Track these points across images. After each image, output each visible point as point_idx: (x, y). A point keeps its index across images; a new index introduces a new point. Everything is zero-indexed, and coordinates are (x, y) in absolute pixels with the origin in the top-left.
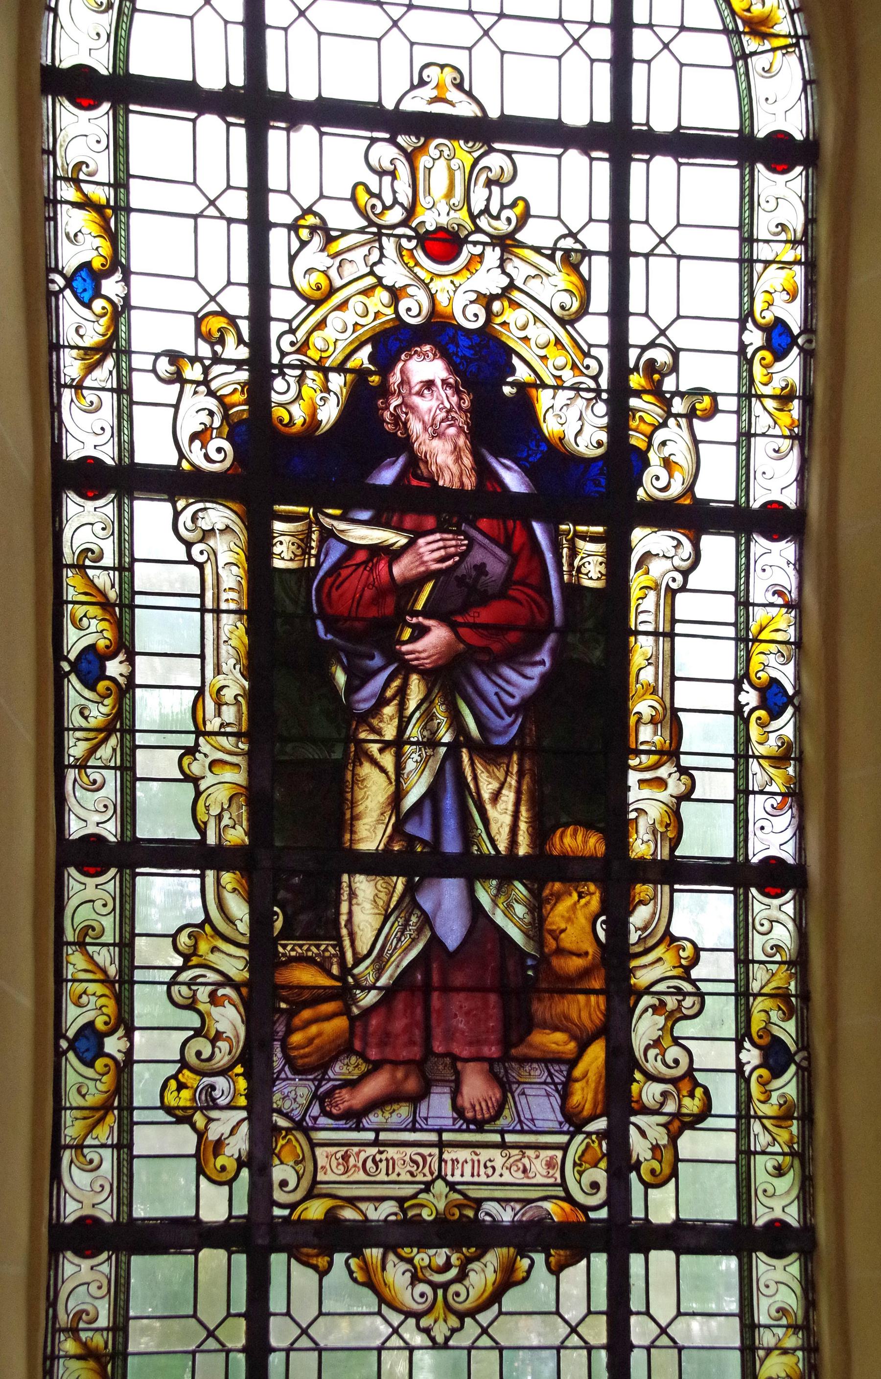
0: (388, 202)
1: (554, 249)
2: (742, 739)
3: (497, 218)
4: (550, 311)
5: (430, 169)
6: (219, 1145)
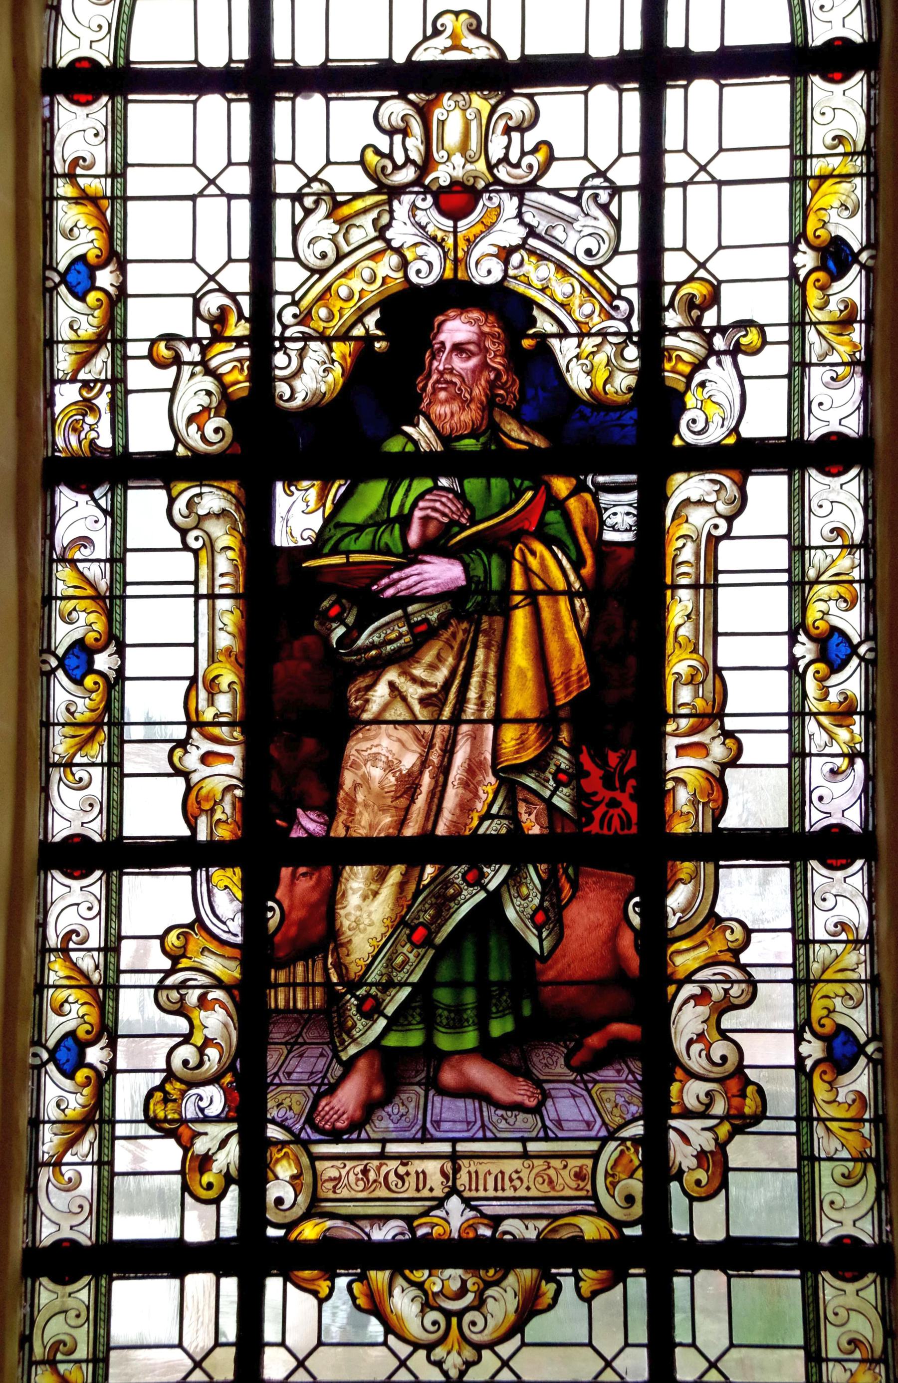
0: (400, 160)
1: (581, 189)
2: (797, 694)
3: (518, 166)
4: (574, 258)
5: (443, 122)
6: (205, 1162)
